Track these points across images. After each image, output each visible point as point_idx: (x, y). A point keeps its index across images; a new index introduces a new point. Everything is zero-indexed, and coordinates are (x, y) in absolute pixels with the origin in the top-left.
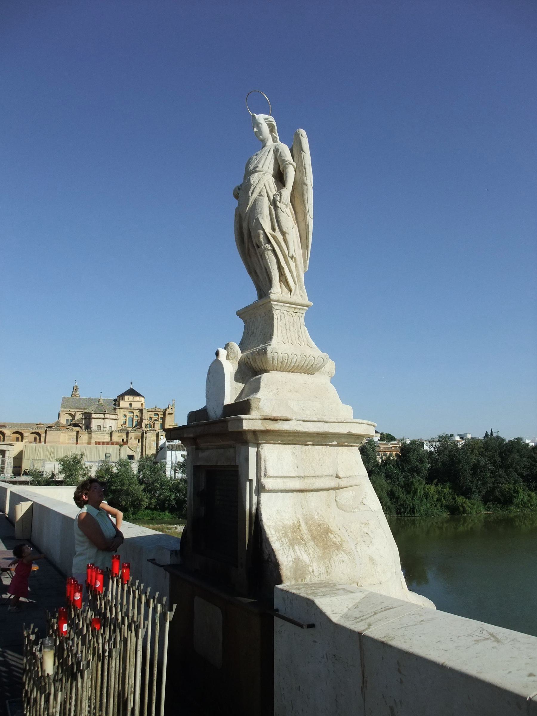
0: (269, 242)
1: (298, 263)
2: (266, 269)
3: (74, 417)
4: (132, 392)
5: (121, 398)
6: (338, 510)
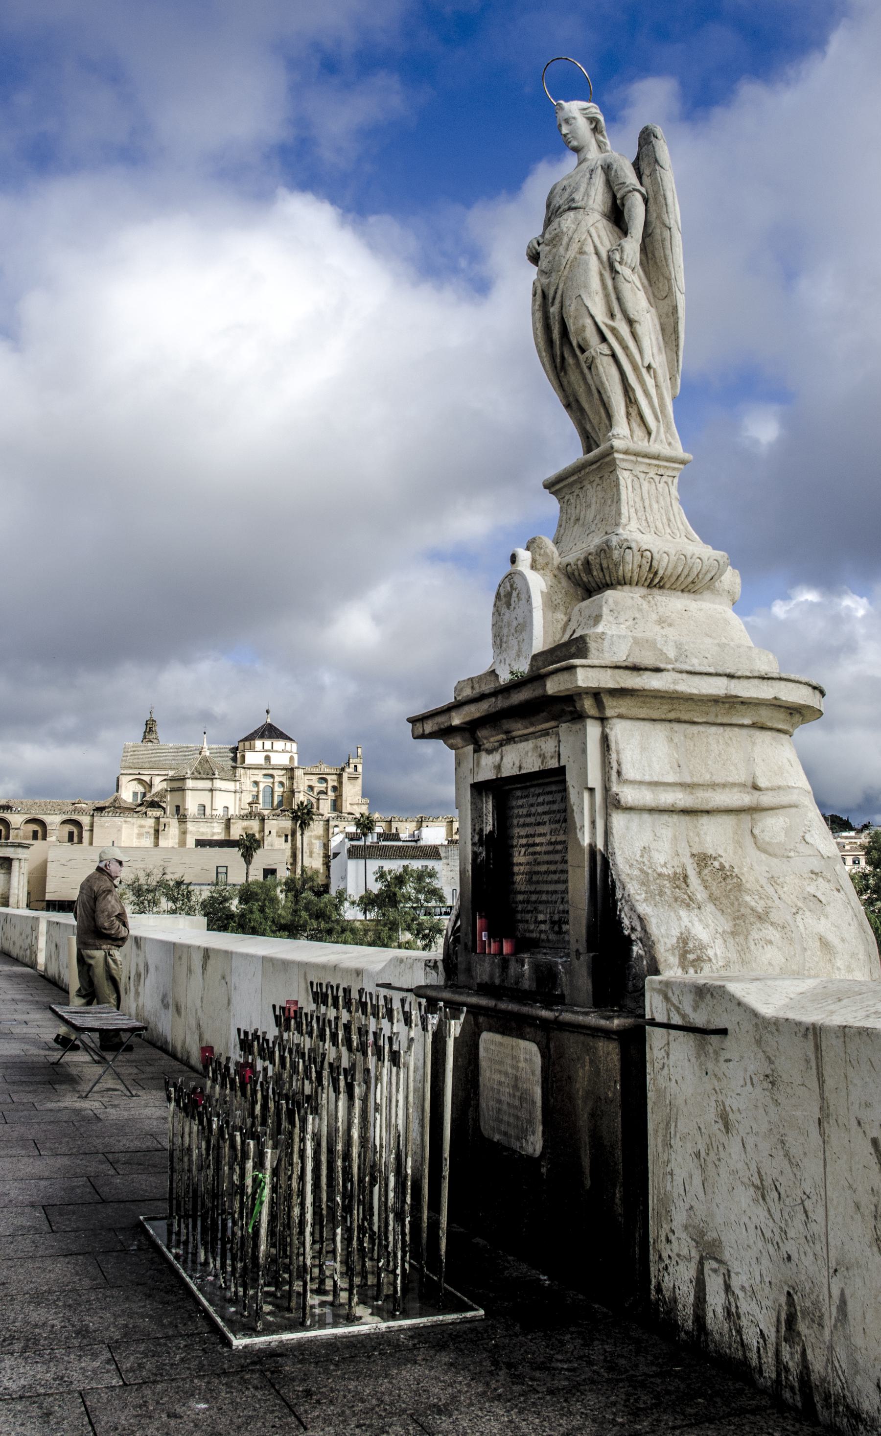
0: (604, 339)
1: (661, 379)
2: (599, 392)
4: (270, 732)
5: (247, 743)
6: (758, 853)
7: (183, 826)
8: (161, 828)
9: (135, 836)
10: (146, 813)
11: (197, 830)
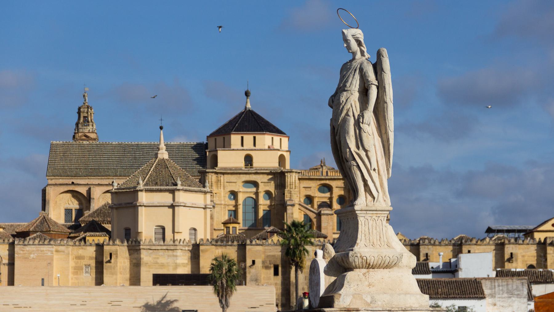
0: (354, 159)
3: (85, 200)
4: (251, 122)
5: (220, 139)
7: (136, 255)
8: (106, 258)
9: (71, 270)
10: (84, 239)
11: (154, 262)
